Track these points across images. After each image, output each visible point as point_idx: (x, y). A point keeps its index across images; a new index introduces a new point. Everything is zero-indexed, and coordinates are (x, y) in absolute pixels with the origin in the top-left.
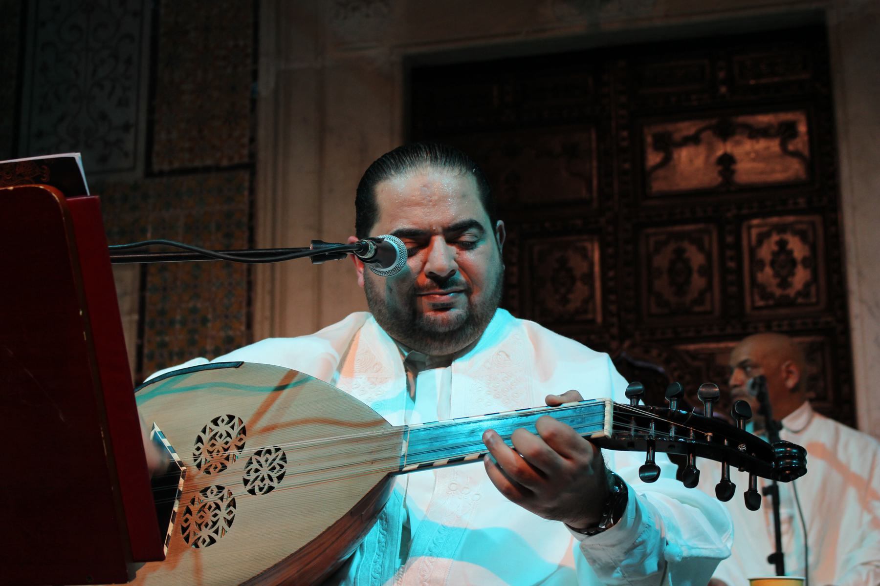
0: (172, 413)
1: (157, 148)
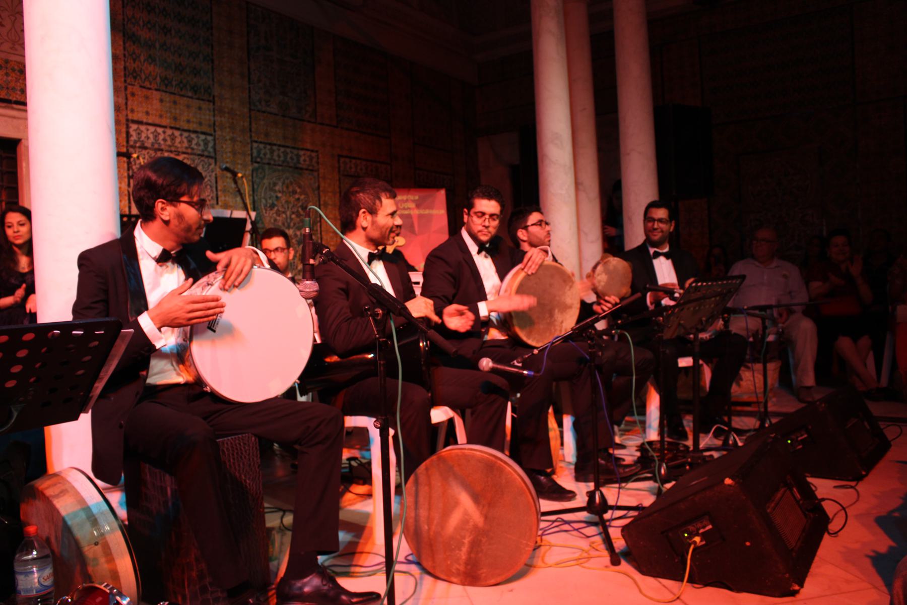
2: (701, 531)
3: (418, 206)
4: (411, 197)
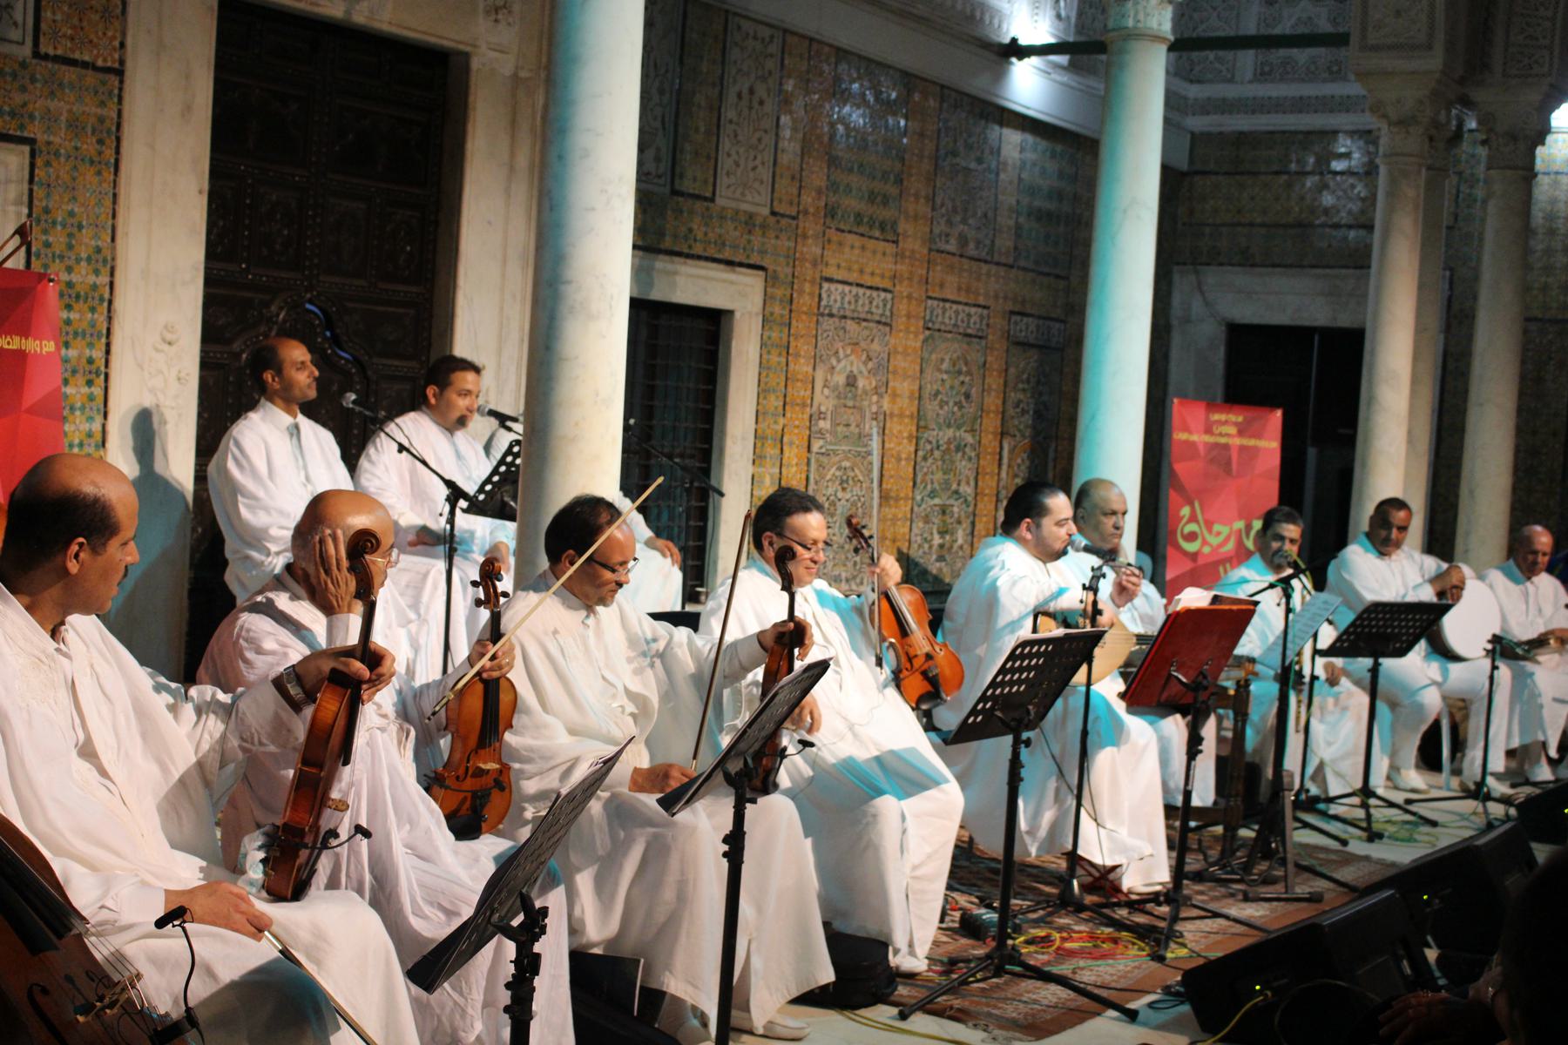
0: (1248, 759)
1: (43, 26)
2: (1275, 984)
3: (1241, 433)
4: (1232, 418)
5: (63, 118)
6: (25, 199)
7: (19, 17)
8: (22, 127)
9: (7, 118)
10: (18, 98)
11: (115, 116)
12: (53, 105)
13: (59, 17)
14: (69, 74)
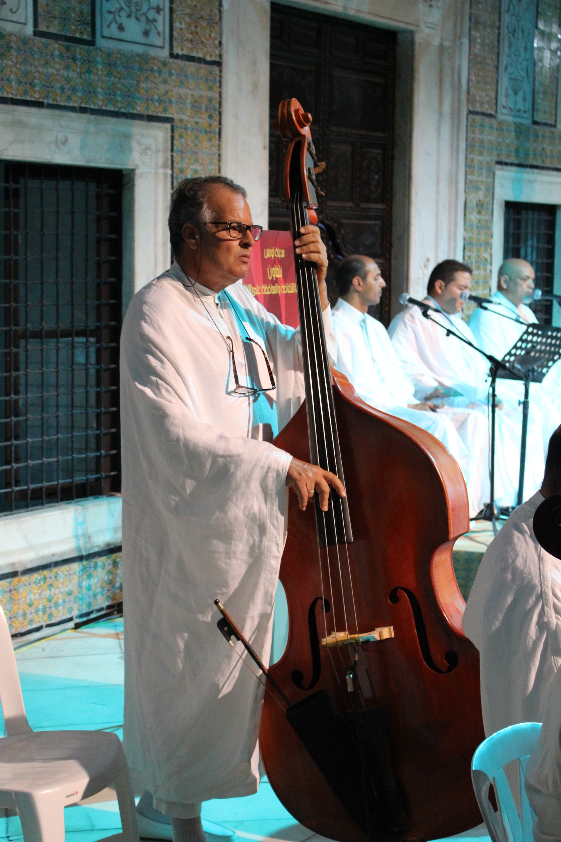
1: (175, 34)
5: (188, 101)
6: (169, 163)
7: (160, 28)
8: (165, 110)
9: (157, 104)
10: (163, 88)
11: (217, 96)
12: (183, 91)
13: (183, 26)
14: (191, 67)
